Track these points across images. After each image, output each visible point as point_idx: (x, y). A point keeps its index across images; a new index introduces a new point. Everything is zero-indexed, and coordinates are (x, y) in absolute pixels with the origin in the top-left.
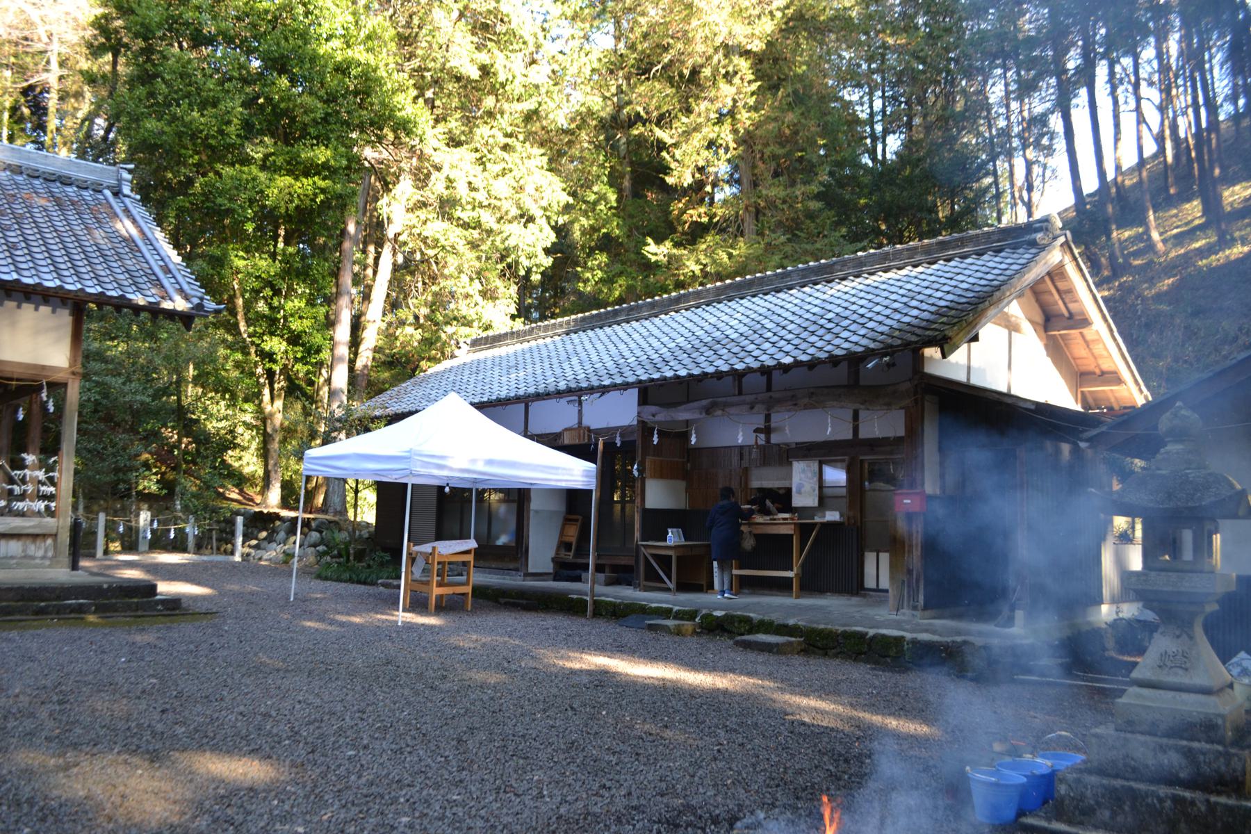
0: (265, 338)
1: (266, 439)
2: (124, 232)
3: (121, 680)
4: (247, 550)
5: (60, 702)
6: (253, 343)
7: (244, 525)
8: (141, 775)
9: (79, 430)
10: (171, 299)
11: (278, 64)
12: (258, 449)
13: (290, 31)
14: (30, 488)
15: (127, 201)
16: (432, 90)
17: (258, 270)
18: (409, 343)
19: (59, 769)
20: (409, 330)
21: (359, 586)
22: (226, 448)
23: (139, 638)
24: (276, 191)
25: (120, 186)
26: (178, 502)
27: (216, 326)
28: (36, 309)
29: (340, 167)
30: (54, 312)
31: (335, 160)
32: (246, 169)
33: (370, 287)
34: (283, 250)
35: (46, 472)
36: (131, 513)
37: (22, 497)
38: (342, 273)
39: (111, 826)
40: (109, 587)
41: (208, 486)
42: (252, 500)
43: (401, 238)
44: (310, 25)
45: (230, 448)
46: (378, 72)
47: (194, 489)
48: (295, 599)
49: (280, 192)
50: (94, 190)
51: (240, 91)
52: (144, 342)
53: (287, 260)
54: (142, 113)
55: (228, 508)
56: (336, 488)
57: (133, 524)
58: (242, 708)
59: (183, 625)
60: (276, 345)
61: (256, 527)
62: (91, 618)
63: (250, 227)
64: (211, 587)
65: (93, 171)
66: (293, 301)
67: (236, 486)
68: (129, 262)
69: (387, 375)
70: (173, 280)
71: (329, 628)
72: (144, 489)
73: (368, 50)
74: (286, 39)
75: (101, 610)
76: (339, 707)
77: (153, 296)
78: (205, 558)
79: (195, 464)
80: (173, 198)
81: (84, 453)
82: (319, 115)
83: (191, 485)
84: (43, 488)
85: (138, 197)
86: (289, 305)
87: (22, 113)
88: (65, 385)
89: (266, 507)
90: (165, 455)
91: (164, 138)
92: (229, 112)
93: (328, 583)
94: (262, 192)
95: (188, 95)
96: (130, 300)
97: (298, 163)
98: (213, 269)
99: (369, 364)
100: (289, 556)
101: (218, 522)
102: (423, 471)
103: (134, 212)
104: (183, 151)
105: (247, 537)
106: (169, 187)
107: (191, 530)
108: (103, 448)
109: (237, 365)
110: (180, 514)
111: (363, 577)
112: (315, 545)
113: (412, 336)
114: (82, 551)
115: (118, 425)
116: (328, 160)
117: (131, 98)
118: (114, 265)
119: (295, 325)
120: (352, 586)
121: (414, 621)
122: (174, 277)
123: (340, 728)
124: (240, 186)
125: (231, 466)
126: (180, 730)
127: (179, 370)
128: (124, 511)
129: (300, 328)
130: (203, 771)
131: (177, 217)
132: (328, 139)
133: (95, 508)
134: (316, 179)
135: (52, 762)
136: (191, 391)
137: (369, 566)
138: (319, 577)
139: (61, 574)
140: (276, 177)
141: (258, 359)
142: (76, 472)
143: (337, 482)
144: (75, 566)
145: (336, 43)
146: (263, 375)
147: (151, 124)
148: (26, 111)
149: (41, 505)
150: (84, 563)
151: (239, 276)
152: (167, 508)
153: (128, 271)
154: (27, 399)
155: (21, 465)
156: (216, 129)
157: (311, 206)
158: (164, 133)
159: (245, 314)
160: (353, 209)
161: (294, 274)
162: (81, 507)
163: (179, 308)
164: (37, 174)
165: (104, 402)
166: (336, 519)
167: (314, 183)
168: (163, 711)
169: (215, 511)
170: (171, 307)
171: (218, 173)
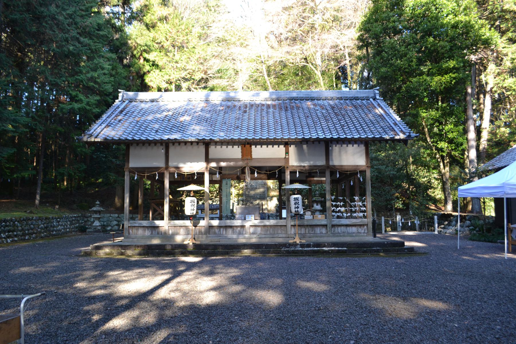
0: (438, 142)
1: (444, 184)
2: (379, 113)
3: (393, 275)
4: (440, 229)
5: (373, 280)
6: (433, 145)
7: (438, 219)
8: (400, 304)
9: (372, 187)
10: (398, 135)
11: (428, 33)
12: (441, 188)
13: (430, 18)
14: (357, 208)
15: (378, 101)
16: (498, 21)
17: (432, 116)
18: (503, 135)
19: (373, 299)
20: (503, 129)
21: (488, 243)
22: (428, 189)
23: (398, 261)
24: (435, 83)
25: (375, 96)
26: (411, 211)
27: (418, 141)
28: (353, 146)
29: (460, 67)
30: (359, 146)
31: (458, 64)
32: (421, 77)
33: (482, 113)
34: (441, 106)
35: (362, 203)
36: (393, 216)
37: (355, 212)
38: (468, 110)
39: (391, 317)
41: (421, 204)
42: (441, 209)
43: (493, 90)
44: (438, 13)
45: (429, 189)
46: (471, 23)
47: (416, 206)
48: (460, 248)
49: (436, 83)
50: (367, 100)
51: (414, 48)
52: (391, 151)
53: (443, 109)
54: (380, 66)
55: (430, 213)
56: (476, 202)
57: (395, 220)
58: (436, 285)
59: (415, 257)
60: (443, 145)
61: (443, 220)
62: (382, 254)
63: (426, 100)
64: (425, 244)
65: (365, 93)
66: (448, 126)
67: (433, 203)
68: (382, 124)
69: (496, 150)
70: (398, 128)
71: (474, 259)
72: (397, 207)
73: (465, 15)
74: (429, 22)
75: (385, 251)
76: (476, 288)
77: (392, 135)
78: (423, 233)
79: (416, 196)
80: (395, 95)
81: (375, 195)
82: (448, 48)
83: (415, 204)
84: (362, 208)
85: (382, 98)
86: (446, 128)
87: (339, 75)
88: (365, 171)
89: (446, 212)
90: (404, 193)
91: (389, 73)
92: (411, 57)
93: (475, 242)
94: (429, 85)
95: (395, 55)
96: (384, 138)
97: (443, 70)
98: (414, 119)
99: (486, 147)
100: (456, 230)
101: (427, 218)
102: (510, 192)
103: (381, 105)
104: (396, 77)
105: (439, 224)
106: (393, 91)
107: (417, 222)
108: (381, 193)
109: (428, 155)
110: (412, 216)
111: (490, 239)
112: (468, 227)
113: (504, 132)
114: (377, 231)
115: (385, 183)
116: (455, 65)
117: (375, 62)
118: (377, 126)
119: (450, 136)
120: (485, 243)
121: (513, 257)
122: (399, 126)
123: (475, 295)
124: (420, 84)
125: (431, 196)
126: (414, 291)
127: (406, 160)
128: (391, 216)
129: (452, 137)
130: (422, 304)
131: (398, 101)
132: (454, 57)
133: (380, 215)
134: (451, 74)
135: (372, 297)
136: (412, 167)
137: (493, 235)
138: (471, 239)
139: (370, 238)
140: (434, 77)
141: (436, 151)
142: (372, 202)
143: (476, 199)
144: (375, 236)
145: (451, 16)
146: (439, 158)
147: (383, 70)
148: (340, 74)
149: (361, 214)
150: (378, 235)
151: (425, 120)
152: (407, 214)
153: (382, 127)
154: (353, 177)
155: (354, 201)
156: (407, 65)
157: (450, 86)
158: (388, 72)
159: (429, 134)
160: (469, 83)
161: (447, 115)
162: (375, 215)
163: (402, 138)
164: (347, 98)
165: (380, 175)
166: (477, 215)
167: (450, 76)
168: (408, 285)
169: (426, 214)
170: (399, 138)
171: (410, 81)
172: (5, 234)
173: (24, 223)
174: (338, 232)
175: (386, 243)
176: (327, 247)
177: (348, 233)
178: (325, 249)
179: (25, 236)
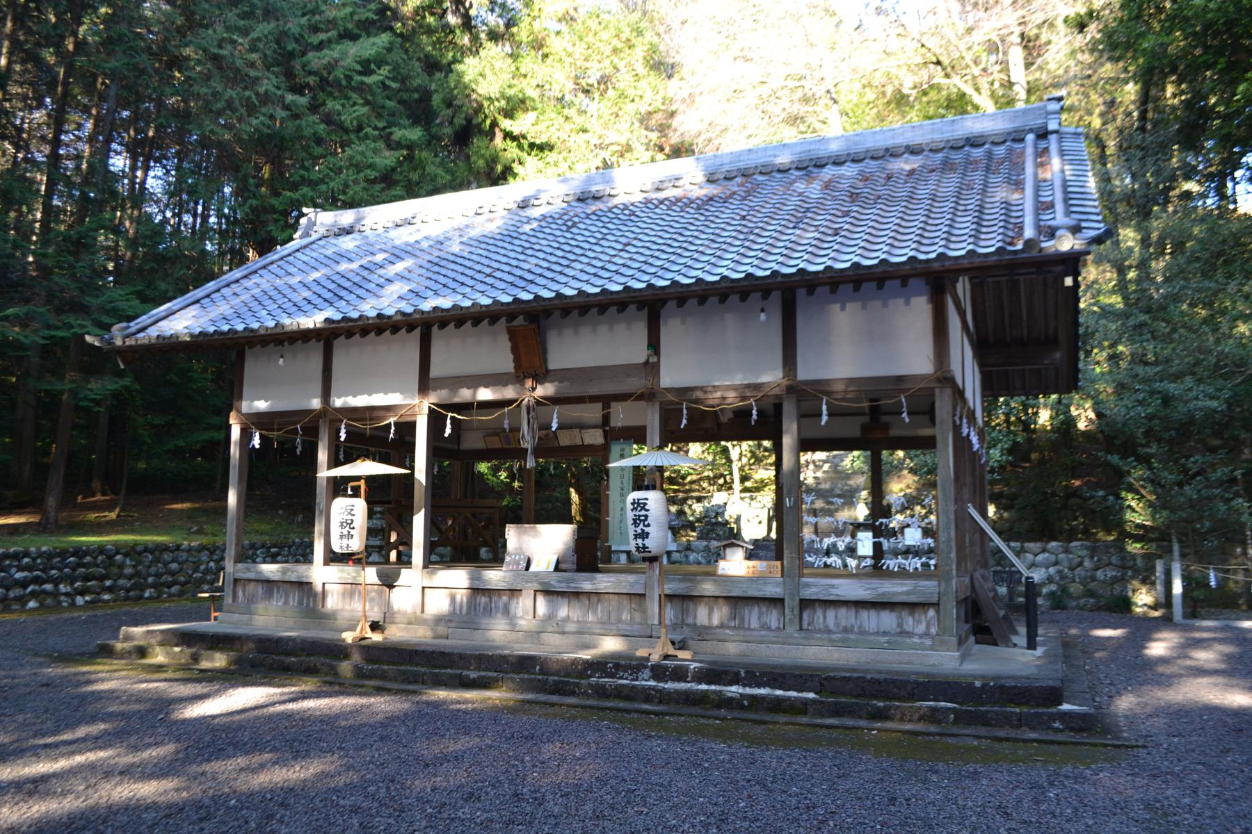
40: (984, 686)
64: (185, 721)
172: (72, 584)
173: (146, 557)
174: (827, 626)
175: (978, 684)
176: (744, 686)
177: (862, 632)
178: (735, 690)
179: (143, 590)
